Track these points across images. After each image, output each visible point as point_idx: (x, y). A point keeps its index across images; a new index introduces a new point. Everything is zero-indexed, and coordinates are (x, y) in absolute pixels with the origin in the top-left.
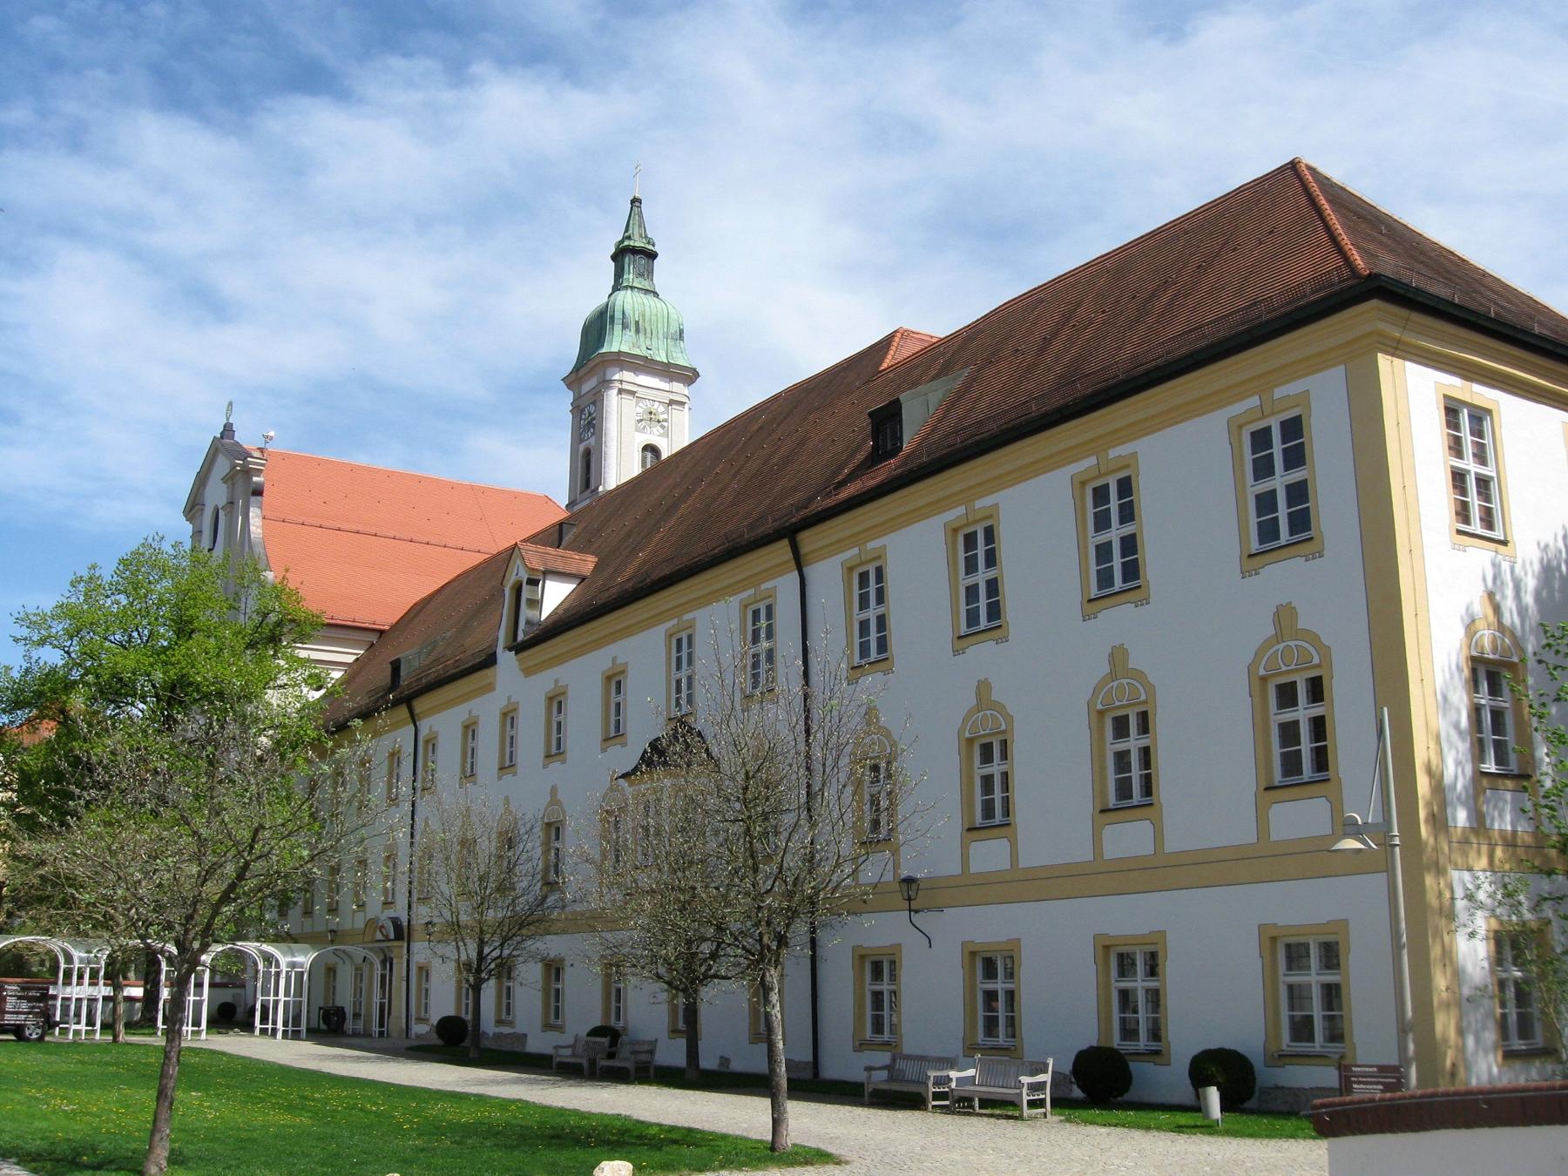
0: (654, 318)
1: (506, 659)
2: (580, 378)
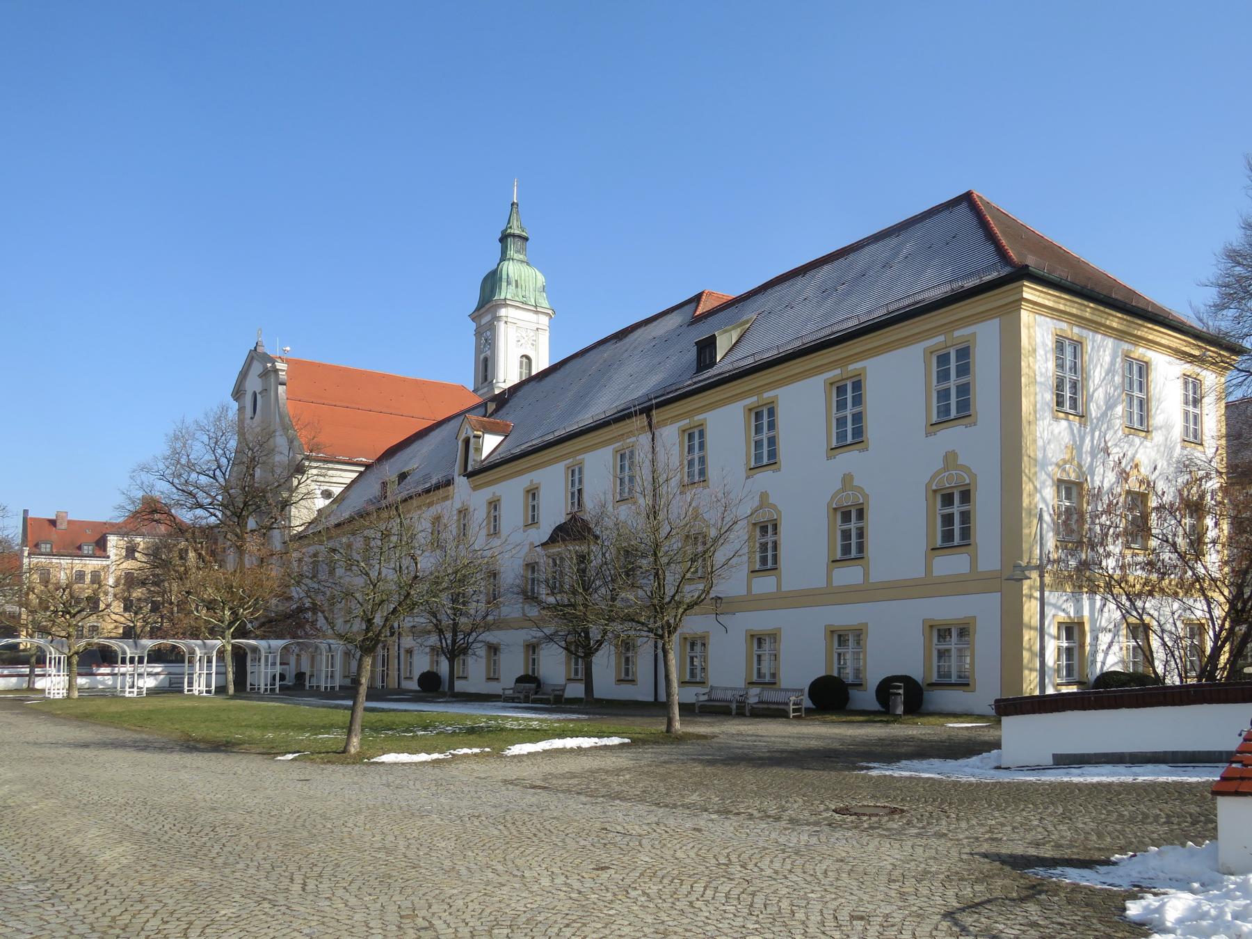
0: (527, 278)
1: (461, 482)
2: (480, 315)
